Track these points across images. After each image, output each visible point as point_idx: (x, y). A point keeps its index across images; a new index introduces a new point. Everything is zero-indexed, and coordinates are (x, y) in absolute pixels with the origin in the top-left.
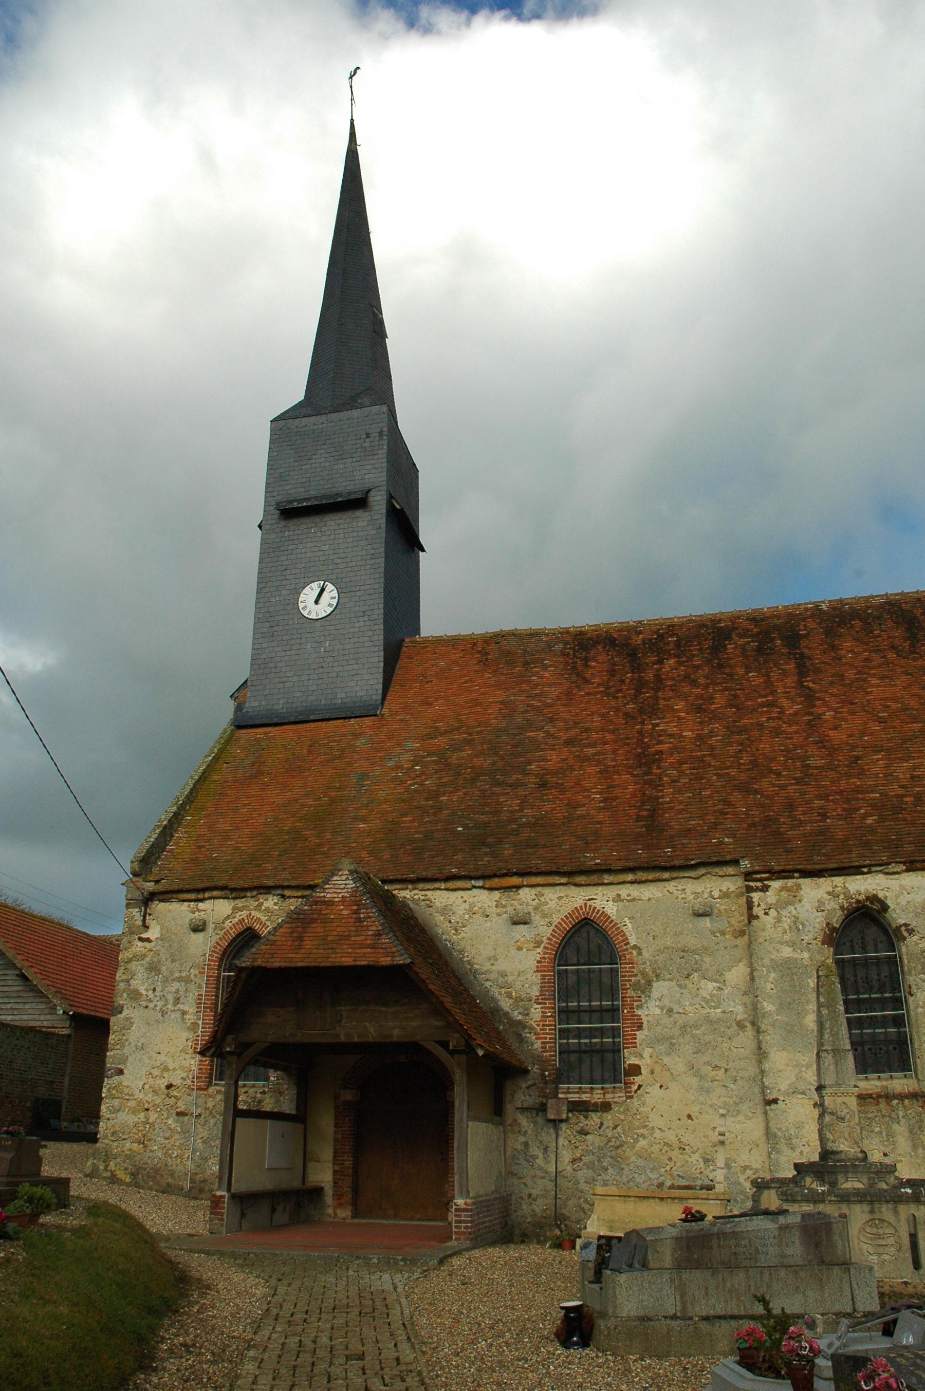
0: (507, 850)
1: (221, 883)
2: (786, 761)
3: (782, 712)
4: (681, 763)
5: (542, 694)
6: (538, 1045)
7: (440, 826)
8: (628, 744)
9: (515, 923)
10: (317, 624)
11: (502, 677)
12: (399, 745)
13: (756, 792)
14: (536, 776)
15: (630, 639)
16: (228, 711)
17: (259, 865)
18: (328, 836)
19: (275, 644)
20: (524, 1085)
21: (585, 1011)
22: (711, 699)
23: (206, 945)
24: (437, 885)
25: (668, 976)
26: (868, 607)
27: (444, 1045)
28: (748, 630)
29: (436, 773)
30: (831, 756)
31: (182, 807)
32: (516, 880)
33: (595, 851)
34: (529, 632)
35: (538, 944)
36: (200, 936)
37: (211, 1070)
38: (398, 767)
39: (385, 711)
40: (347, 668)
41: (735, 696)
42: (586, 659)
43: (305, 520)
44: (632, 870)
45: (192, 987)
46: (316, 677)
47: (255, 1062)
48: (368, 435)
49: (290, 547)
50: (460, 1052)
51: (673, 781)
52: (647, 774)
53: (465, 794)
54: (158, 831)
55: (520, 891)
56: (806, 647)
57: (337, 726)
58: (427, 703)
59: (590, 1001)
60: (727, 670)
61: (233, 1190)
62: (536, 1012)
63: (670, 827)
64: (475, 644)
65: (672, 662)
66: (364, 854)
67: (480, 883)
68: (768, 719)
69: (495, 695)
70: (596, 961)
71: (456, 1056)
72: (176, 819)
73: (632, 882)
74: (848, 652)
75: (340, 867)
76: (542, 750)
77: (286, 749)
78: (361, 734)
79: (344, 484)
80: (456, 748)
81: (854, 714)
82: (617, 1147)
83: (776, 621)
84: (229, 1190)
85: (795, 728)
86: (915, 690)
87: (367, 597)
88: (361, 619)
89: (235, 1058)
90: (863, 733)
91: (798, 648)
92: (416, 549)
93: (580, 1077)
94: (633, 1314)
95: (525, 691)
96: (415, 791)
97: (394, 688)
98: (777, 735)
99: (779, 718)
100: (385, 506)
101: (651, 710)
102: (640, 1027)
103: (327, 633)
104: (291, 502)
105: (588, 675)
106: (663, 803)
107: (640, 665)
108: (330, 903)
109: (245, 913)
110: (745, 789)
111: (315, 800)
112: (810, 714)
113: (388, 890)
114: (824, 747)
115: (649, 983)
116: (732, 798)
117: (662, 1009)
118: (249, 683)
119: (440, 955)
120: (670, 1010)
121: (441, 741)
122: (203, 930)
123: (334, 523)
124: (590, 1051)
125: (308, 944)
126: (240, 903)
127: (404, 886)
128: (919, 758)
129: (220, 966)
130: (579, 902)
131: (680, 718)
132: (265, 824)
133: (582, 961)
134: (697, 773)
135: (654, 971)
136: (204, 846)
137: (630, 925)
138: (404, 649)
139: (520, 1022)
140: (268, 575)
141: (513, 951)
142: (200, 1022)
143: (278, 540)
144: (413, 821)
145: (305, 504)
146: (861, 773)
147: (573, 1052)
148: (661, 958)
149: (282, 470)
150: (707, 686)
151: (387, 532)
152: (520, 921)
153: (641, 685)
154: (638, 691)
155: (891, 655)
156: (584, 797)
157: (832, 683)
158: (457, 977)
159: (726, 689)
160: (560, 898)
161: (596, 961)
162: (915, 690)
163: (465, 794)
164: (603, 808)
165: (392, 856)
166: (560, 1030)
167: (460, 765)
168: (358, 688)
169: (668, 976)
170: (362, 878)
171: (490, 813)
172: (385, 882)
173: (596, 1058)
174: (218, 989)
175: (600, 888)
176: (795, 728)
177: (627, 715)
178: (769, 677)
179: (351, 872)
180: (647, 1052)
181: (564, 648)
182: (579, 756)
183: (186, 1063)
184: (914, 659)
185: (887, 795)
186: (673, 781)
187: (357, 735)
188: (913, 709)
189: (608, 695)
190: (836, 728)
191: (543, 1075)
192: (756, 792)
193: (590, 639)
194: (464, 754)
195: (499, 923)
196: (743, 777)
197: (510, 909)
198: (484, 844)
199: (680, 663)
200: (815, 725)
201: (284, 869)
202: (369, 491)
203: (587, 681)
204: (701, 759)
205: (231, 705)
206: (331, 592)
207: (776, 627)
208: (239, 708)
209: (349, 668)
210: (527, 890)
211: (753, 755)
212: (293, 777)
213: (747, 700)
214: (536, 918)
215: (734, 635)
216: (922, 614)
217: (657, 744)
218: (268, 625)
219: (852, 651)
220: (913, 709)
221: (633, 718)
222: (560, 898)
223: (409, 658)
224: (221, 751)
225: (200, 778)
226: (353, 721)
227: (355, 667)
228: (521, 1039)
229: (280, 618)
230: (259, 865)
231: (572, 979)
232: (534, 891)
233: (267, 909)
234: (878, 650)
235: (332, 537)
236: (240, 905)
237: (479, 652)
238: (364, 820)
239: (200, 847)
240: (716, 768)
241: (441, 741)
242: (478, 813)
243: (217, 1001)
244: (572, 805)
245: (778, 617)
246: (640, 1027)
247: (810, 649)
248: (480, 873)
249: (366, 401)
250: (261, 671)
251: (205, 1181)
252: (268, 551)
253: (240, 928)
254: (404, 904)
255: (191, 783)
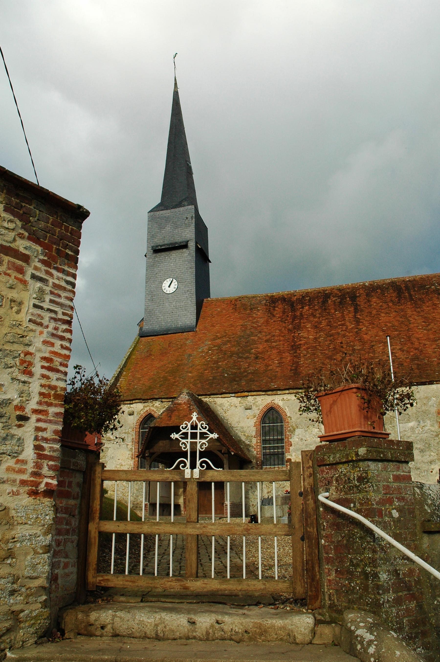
0: (243, 383)
1: (139, 397)
2: (346, 347)
3: (347, 328)
4: (308, 348)
5: (257, 322)
6: (255, 452)
7: (219, 374)
8: (289, 341)
9: (246, 409)
10: (170, 295)
11: (242, 315)
12: (203, 343)
13: (335, 359)
14: (254, 354)
15: (291, 298)
16: (137, 330)
17: (153, 390)
18: (178, 379)
19: (154, 303)
20: (250, 467)
21: (271, 440)
22: (320, 323)
23: (134, 420)
24: (218, 396)
25: (301, 427)
26: (384, 284)
27: (220, 451)
28: (337, 294)
29: (217, 354)
30: (363, 345)
31: (122, 369)
32: (246, 394)
33: (275, 382)
34: (252, 296)
35: (255, 416)
36: (132, 416)
37: (138, 465)
38: (203, 352)
39: (197, 329)
40: (182, 313)
41: (330, 322)
42: (274, 307)
43: (163, 253)
44: (288, 389)
45: (130, 435)
46: (170, 316)
47: (155, 460)
48: (187, 218)
49: (158, 265)
50: (226, 453)
51: (304, 356)
52: (295, 353)
53: (228, 362)
54: (114, 379)
55: (248, 398)
56: (358, 301)
57: (179, 336)
58: (213, 326)
59: (274, 436)
60: (327, 311)
61: (150, 502)
62: (254, 441)
63: (303, 373)
64: (231, 301)
65: (307, 308)
66: (191, 385)
67: (233, 395)
68: (342, 331)
69: (239, 322)
70: (276, 422)
71: (225, 455)
72: (120, 373)
73: (288, 394)
74: (374, 303)
75: (183, 391)
76: (257, 344)
77: (160, 345)
78: (188, 339)
79: (178, 238)
80: (225, 344)
81: (374, 328)
82: (283, 488)
83: (348, 291)
84: (149, 502)
85: (351, 334)
86: (398, 318)
87: (189, 284)
88: (187, 293)
89: (149, 458)
90: (376, 336)
91: (355, 301)
92: (208, 262)
93: (270, 463)
94: (269, 516)
95: (251, 320)
96: (209, 361)
97: (200, 320)
98: (344, 337)
99: (345, 330)
100: (194, 248)
101: (298, 327)
102: (291, 445)
103: (173, 299)
104: (157, 246)
105: (275, 313)
106: (300, 364)
107: (294, 309)
108: (180, 404)
109: (148, 408)
110: (330, 358)
111: (172, 365)
112: (357, 328)
113: (200, 399)
114: (361, 342)
115: (294, 430)
116: (325, 362)
117: (299, 439)
118: (144, 319)
119: (219, 421)
120: (302, 439)
121: (218, 341)
122: (133, 415)
123: (174, 254)
124: (274, 454)
125: (173, 418)
126: (146, 404)
127: (206, 397)
128: (395, 345)
129: (140, 428)
130: (269, 401)
131: (308, 331)
132: (154, 375)
133: (270, 422)
134: (313, 353)
135: (296, 425)
136: (131, 384)
137: (287, 409)
138: (204, 304)
139: (248, 445)
140: (150, 276)
141: (246, 419)
142: (133, 448)
143: (153, 262)
144: (209, 372)
145: (163, 247)
146: (374, 352)
147: (268, 455)
148: (299, 421)
149: (154, 233)
150: (319, 318)
151: (196, 258)
152: (248, 408)
153: (294, 317)
154: (294, 320)
155: (390, 304)
156: (272, 362)
157: (367, 316)
158: (225, 429)
159: (327, 319)
160: (262, 400)
161: (276, 422)
162: (398, 318)
163: (228, 362)
164: (278, 366)
165: (201, 386)
166: (263, 447)
167: (226, 351)
168: (186, 321)
169: (301, 427)
170: (191, 395)
171: (237, 369)
172: (199, 395)
173: (276, 457)
174: (139, 436)
175: (277, 396)
176: (351, 334)
177: (289, 330)
178: (343, 313)
179: (187, 393)
180: (294, 454)
181: (266, 302)
182: (270, 346)
183: (129, 463)
184: (399, 306)
185: (382, 360)
186: (304, 356)
187: (187, 339)
188: (396, 326)
189: (282, 322)
190: (366, 334)
191: (257, 463)
192: (335, 359)
193: (276, 298)
194: (227, 346)
195: (240, 409)
196: (330, 354)
197: (244, 404)
198: (235, 381)
199: (310, 308)
200: (359, 333)
201: (162, 392)
202: (188, 241)
203: (274, 316)
204: (315, 347)
205: (138, 328)
206: (175, 283)
207: (348, 293)
208: (141, 329)
209: (183, 312)
210: (250, 397)
211: (334, 345)
212: (163, 356)
213: (334, 323)
214: (254, 407)
215: (331, 296)
216: (404, 287)
217: (299, 341)
218: (150, 296)
219: (376, 303)
220: (396, 326)
221: (291, 331)
222: (262, 400)
223: (206, 307)
224: (135, 347)
225: (128, 357)
226: (185, 333)
227: (185, 312)
228: (249, 451)
229: (155, 293)
230: (153, 390)
231: (267, 428)
232: (253, 397)
233: (156, 406)
234: (386, 302)
235: (174, 260)
236: (146, 405)
237: (233, 304)
238: (190, 372)
239: (130, 384)
240: (320, 350)
241: (218, 341)
242: (233, 369)
243: (139, 440)
244: (267, 365)
245: (349, 288)
246: (291, 445)
247: (360, 301)
248: (233, 392)
249: (186, 203)
250: (148, 315)
251: (138, 504)
252: (150, 267)
253: (147, 414)
254: (206, 403)
255: (125, 360)
